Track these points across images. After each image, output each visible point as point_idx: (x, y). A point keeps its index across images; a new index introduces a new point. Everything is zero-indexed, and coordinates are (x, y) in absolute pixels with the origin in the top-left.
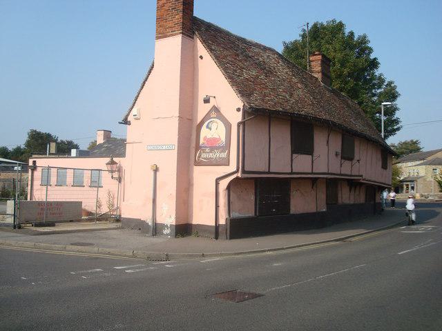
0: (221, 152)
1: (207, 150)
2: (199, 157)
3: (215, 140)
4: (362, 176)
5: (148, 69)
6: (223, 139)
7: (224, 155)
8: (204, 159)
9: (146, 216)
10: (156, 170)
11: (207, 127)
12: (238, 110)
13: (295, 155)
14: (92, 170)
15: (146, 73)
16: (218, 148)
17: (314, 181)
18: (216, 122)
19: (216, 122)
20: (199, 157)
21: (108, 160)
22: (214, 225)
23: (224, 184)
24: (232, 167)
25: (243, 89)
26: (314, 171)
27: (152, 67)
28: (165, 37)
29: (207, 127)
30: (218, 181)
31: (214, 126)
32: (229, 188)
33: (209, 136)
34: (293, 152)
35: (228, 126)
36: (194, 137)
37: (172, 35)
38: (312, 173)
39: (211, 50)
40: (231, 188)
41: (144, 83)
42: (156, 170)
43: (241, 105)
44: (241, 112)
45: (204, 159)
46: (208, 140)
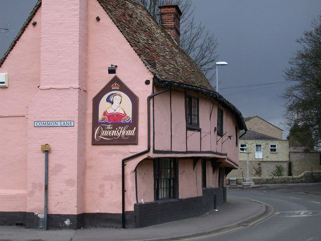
0: (127, 130)
1: (109, 127)
2: (99, 134)
3: (119, 116)
4: (226, 155)
5: (22, 26)
6: (129, 114)
7: (131, 133)
8: (104, 136)
10: (47, 151)
12: (147, 82)
13: (189, 132)
15: (8, 48)
16: (123, 125)
17: (195, 160)
18: (120, 95)
19: (120, 95)
20: (99, 134)
22: (122, 213)
23: (132, 165)
25: (150, 63)
26: (202, 150)
27: (39, 6)
29: (108, 100)
30: (124, 162)
31: (116, 99)
34: (188, 129)
35: (134, 99)
38: (187, 152)
39: (109, 11)
40: (138, 170)
41: (15, 43)
42: (47, 151)
43: (150, 77)
45: (104, 136)
46: (111, 116)
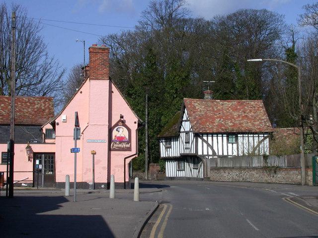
1: (118, 143)
3: (122, 138)
7: (128, 146)
9: (88, 179)
10: (94, 154)
11: (117, 130)
12: (135, 123)
14: (110, 150)
16: (124, 142)
21: (26, 145)
22: (123, 182)
23: (128, 161)
24: (134, 151)
28: (98, 79)
29: (117, 130)
31: (121, 130)
32: (129, 164)
33: (118, 135)
35: (129, 130)
36: (184, 182)
37: (102, 79)
42: (94, 154)
44: (137, 124)
